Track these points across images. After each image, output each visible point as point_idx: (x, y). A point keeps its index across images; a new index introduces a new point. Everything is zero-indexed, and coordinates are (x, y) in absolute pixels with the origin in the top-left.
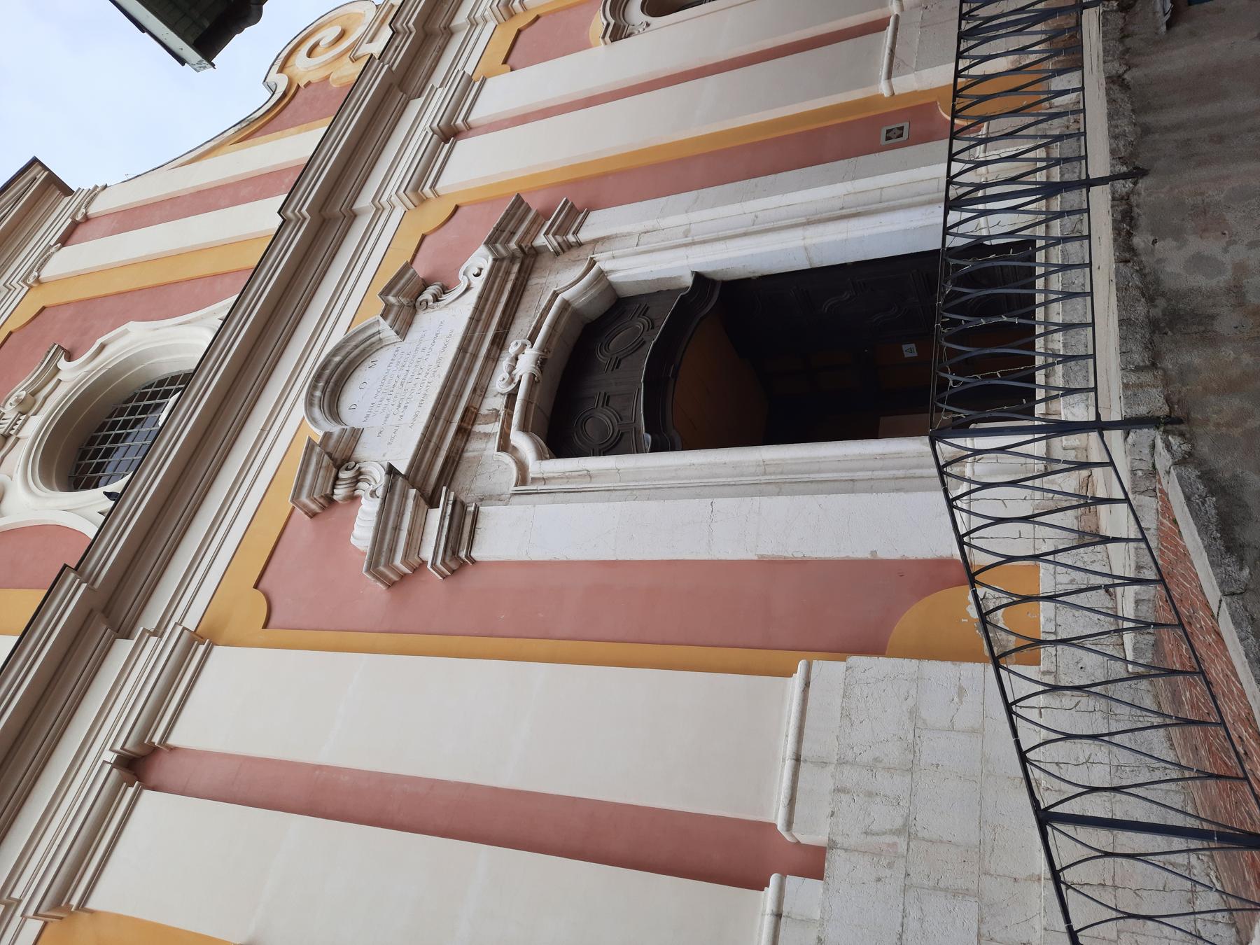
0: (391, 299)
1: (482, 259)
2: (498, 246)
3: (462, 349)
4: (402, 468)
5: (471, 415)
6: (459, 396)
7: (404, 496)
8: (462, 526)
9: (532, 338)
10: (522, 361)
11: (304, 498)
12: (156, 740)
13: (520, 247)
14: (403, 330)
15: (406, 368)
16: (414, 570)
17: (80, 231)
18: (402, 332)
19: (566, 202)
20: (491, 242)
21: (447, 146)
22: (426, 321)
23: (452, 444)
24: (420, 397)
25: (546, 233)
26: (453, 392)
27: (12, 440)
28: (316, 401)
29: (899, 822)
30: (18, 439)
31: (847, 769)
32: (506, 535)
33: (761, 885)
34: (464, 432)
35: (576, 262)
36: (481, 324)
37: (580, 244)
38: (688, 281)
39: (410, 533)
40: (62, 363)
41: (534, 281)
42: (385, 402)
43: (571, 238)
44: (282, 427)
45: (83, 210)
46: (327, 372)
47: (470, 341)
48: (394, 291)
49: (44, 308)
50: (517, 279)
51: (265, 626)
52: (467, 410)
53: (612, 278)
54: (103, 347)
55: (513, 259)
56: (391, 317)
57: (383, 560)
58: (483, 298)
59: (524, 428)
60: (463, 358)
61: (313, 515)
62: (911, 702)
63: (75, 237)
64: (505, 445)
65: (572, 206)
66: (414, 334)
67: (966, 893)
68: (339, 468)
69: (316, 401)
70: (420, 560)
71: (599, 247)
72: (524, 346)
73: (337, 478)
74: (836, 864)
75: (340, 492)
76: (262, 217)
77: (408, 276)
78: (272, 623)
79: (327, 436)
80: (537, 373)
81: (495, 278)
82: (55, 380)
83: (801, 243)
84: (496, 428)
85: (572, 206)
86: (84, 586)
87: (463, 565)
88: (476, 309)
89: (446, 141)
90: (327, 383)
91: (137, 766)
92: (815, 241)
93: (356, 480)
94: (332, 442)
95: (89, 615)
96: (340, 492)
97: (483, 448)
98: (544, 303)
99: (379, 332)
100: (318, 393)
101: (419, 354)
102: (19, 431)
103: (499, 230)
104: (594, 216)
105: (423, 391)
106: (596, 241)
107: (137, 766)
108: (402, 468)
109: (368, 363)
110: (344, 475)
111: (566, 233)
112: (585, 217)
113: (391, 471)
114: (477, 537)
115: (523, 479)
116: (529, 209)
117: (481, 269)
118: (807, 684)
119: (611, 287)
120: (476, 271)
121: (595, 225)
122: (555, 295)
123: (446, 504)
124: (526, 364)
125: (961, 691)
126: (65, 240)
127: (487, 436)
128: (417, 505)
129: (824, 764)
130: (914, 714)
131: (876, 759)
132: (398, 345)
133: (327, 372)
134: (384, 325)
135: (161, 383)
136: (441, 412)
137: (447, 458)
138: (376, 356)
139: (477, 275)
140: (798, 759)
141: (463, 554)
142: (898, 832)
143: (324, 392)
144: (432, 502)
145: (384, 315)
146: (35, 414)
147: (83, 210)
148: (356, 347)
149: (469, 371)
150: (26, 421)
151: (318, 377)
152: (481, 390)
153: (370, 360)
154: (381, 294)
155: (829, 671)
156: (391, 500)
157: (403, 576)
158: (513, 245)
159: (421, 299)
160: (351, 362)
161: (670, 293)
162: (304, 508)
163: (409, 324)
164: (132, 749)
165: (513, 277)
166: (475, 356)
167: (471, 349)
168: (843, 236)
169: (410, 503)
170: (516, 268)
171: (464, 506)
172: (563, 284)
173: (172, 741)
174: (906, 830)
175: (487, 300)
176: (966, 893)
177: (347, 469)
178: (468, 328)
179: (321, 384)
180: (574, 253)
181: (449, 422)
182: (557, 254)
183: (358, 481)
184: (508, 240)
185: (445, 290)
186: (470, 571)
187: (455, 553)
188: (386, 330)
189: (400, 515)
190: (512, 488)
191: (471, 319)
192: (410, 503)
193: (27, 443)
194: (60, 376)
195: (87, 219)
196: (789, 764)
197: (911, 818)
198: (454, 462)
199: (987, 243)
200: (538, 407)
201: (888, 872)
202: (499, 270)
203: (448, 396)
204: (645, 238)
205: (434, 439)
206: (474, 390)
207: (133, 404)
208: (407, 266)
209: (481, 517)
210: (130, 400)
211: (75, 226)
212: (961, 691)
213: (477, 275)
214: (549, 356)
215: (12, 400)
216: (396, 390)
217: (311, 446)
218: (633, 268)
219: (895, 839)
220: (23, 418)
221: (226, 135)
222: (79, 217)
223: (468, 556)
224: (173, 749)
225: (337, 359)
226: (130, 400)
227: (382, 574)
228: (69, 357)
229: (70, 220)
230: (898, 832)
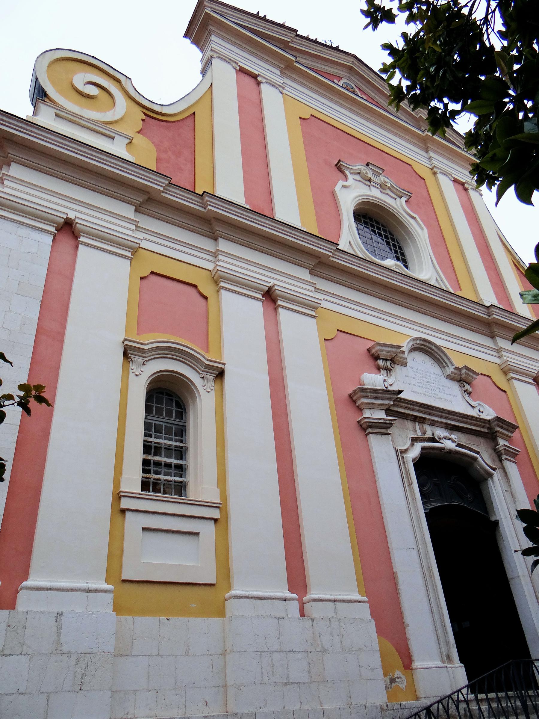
0: (464, 371)
1: (489, 414)
2: (496, 423)
3: (450, 412)
4: (401, 396)
5: (422, 421)
6: (430, 414)
7: (390, 399)
8: (382, 428)
9: (459, 445)
10: (449, 442)
11: (378, 348)
12: (280, 303)
13: (497, 432)
14: (450, 377)
15: (435, 382)
16: (358, 407)
17: (460, 188)
18: (449, 377)
19: (519, 451)
20: (498, 419)
21: (532, 381)
22: (455, 387)
23: (410, 415)
24: (425, 393)
25: (505, 445)
26: (431, 411)
27: (368, 183)
28: (415, 342)
29: (326, 647)
30: (369, 186)
31: (337, 623)
32: (381, 449)
33: (291, 589)
34: (415, 419)
35: (493, 460)
36: (461, 419)
37: (501, 461)
38: (493, 519)
39: (374, 404)
40: (404, 199)
41: (481, 440)
42: (419, 375)
43: (504, 457)
44: (400, 327)
45: (264, 81)
46: (427, 344)
47: (454, 415)
48: (467, 372)
49: (424, 180)
50: (482, 432)
51: (325, 339)
52: (424, 418)
53: (490, 480)
54: (414, 218)
55: (490, 428)
56: (456, 371)
57: (363, 394)
58: (472, 418)
59: (423, 449)
60: (446, 413)
61: (369, 350)
62: (365, 648)
63: (457, 185)
64: (414, 440)
65: (517, 454)
66: (446, 380)
67: (311, 677)
68: (391, 360)
69: (415, 342)
70: (369, 412)
71: (502, 471)
72: (455, 442)
73: (387, 360)
74: (307, 623)
75: (381, 363)
76: (489, 297)
77: (474, 376)
78: (327, 342)
79: (404, 352)
80: (445, 451)
81: (481, 422)
82: (395, 197)
83: (520, 574)
84: (419, 435)
85: (517, 454)
86: (331, 254)
87: (364, 430)
88: (467, 415)
89: (534, 380)
90: (423, 345)
91: (270, 296)
92: (523, 582)
93: (388, 370)
94: (401, 355)
95: (316, 256)
96: (381, 363)
97: (412, 430)
98: (473, 447)
99: (448, 366)
100: (418, 342)
101: (441, 388)
102: (373, 186)
103: (503, 421)
104: (514, 465)
105: (427, 394)
106: (504, 469)
107: (270, 296)
108: (401, 396)
109: (433, 362)
110: (389, 363)
111: (506, 454)
112: (513, 462)
113: (400, 392)
114: (378, 436)
115: (404, 452)
116: (512, 432)
117: (482, 412)
118: (360, 602)
119: (485, 480)
120: (481, 410)
121: (512, 468)
122: (478, 453)
123: (390, 420)
124: (449, 445)
125: (373, 670)
126: (456, 181)
127: (415, 430)
128: (386, 405)
129: (336, 612)
130: (361, 650)
131: (343, 635)
132: (443, 375)
133: (427, 344)
134: (452, 369)
135: (400, 248)
136: (423, 407)
137: (407, 414)
138: (436, 365)
139: (479, 411)
140: (335, 601)
141: (370, 430)
142: (323, 647)
143: (419, 344)
144: (389, 412)
145: (456, 368)
146: (381, 191)
147: (264, 81)
148: (440, 356)
149: (441, 417)
150: (377, 188)
151: (425, 340)
152: (433, 423)
153: (435, 363)
154: (466, 366)
155: (365, 611)
156: (388, 394)
157: (355, 402)
158: (497, 429)
159: (465, 383)
160: (432, 354)
161: (486, 511)
162: (373, 347)
163: (453, 379)
164: (274, 293)
165: (482, 430)
166: (447, 418)
167: (450, 416)
168: (527, 595)
169: (387, 402)
170: (486, 430)
171: (389, 428)
172: (484, 458)
173: (281, 310)
174: (324, 651)
175: (471, 420)
176: (311, 677)
177: (391, 364)
178: (459, 413)
179: (422, 343)
180: (496, 459)
181: (419, 411)
182: (495, 450)
183: (386, 370)
184: (499, 426)
185: (469, 394)
186: (362, 434)
187: (369, 427)
188: (450, 369)
189: (382, 399)
190: (399, 448)
191: (463, 414)
192: (387, 402)
193: (369, 193)
194: (398, 199)
195: (259, 83)
196: (332, 597)
197: (328, 652)
198: (403, 416)
199: (533, 666)
200: (430, 453)
201: (310, 644)
202: (484, 423)
203: (430, 409)
204: (509, 494)
205: (412, 406)
206: (433, 420)
207: (389, 236)
208: (477, 374)
209: (386, 436)
210: (391, 234)
211: (255, 77)
212: (373, 670)
213: (479, 411)
214: (452, 455)
215: (386, 180)
216: (425, 379)
217: (399, 347)
218: (496, 489)
219: (320, 646)
220: (379, 187)
221: (516, 255)
222: (466, 186)
223: (369, 433)
224: (276, 309)
225: (434, 348)
226: (391, 234)
227: (356, 393)
228: (406, 201)
229: (257, 73)
230: (323, 647)
